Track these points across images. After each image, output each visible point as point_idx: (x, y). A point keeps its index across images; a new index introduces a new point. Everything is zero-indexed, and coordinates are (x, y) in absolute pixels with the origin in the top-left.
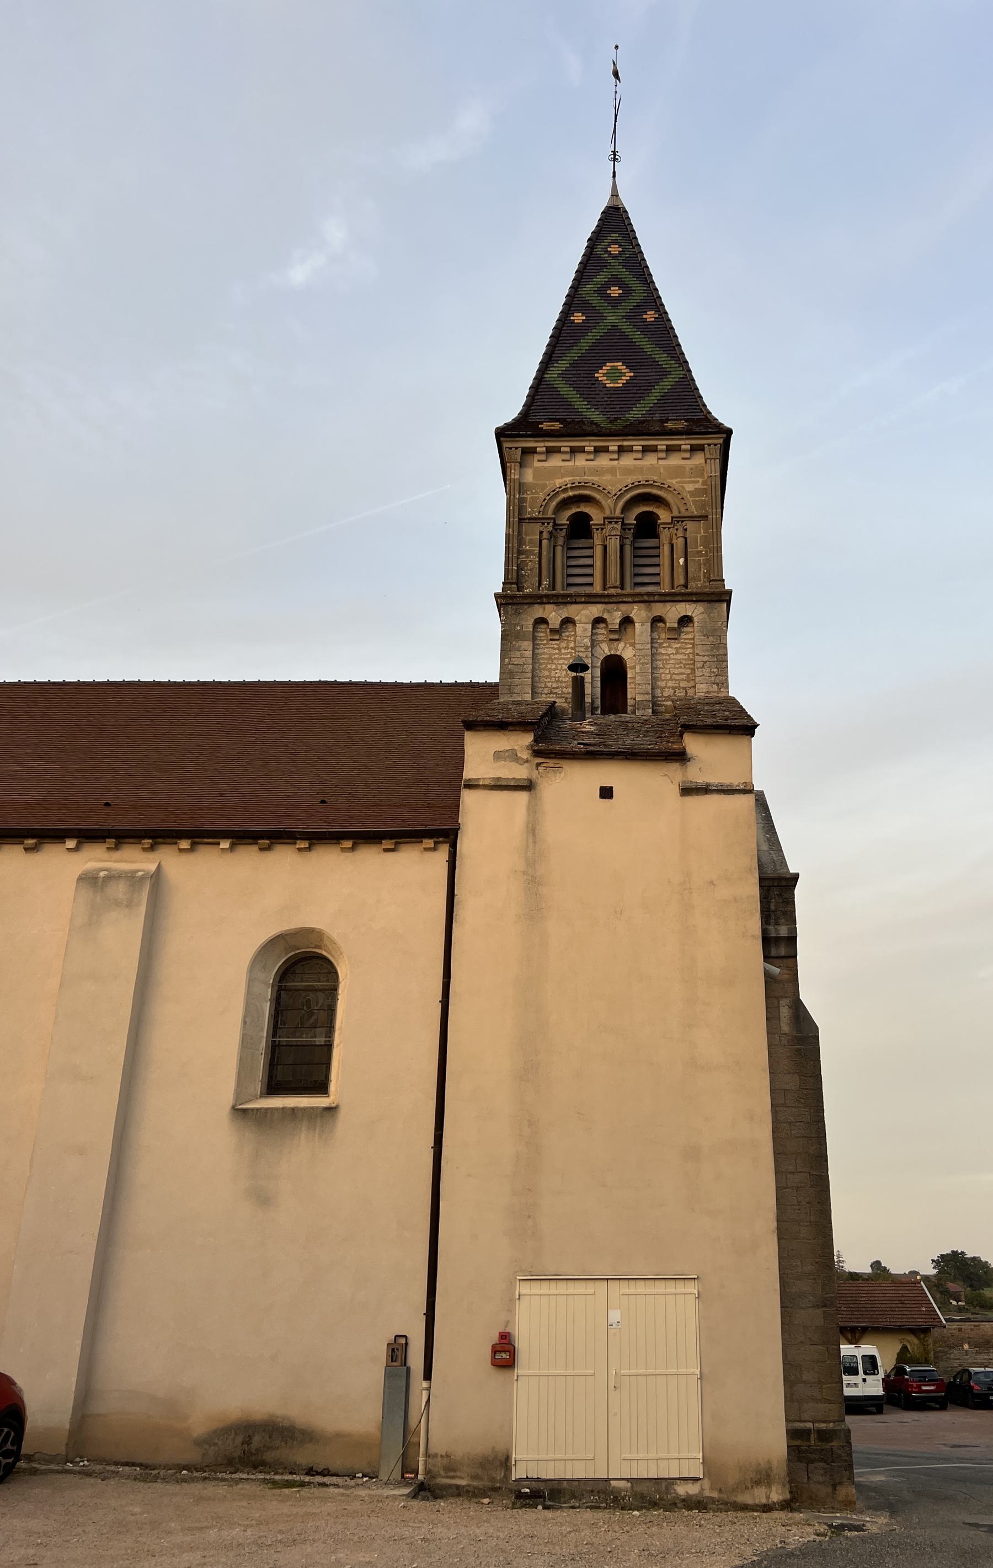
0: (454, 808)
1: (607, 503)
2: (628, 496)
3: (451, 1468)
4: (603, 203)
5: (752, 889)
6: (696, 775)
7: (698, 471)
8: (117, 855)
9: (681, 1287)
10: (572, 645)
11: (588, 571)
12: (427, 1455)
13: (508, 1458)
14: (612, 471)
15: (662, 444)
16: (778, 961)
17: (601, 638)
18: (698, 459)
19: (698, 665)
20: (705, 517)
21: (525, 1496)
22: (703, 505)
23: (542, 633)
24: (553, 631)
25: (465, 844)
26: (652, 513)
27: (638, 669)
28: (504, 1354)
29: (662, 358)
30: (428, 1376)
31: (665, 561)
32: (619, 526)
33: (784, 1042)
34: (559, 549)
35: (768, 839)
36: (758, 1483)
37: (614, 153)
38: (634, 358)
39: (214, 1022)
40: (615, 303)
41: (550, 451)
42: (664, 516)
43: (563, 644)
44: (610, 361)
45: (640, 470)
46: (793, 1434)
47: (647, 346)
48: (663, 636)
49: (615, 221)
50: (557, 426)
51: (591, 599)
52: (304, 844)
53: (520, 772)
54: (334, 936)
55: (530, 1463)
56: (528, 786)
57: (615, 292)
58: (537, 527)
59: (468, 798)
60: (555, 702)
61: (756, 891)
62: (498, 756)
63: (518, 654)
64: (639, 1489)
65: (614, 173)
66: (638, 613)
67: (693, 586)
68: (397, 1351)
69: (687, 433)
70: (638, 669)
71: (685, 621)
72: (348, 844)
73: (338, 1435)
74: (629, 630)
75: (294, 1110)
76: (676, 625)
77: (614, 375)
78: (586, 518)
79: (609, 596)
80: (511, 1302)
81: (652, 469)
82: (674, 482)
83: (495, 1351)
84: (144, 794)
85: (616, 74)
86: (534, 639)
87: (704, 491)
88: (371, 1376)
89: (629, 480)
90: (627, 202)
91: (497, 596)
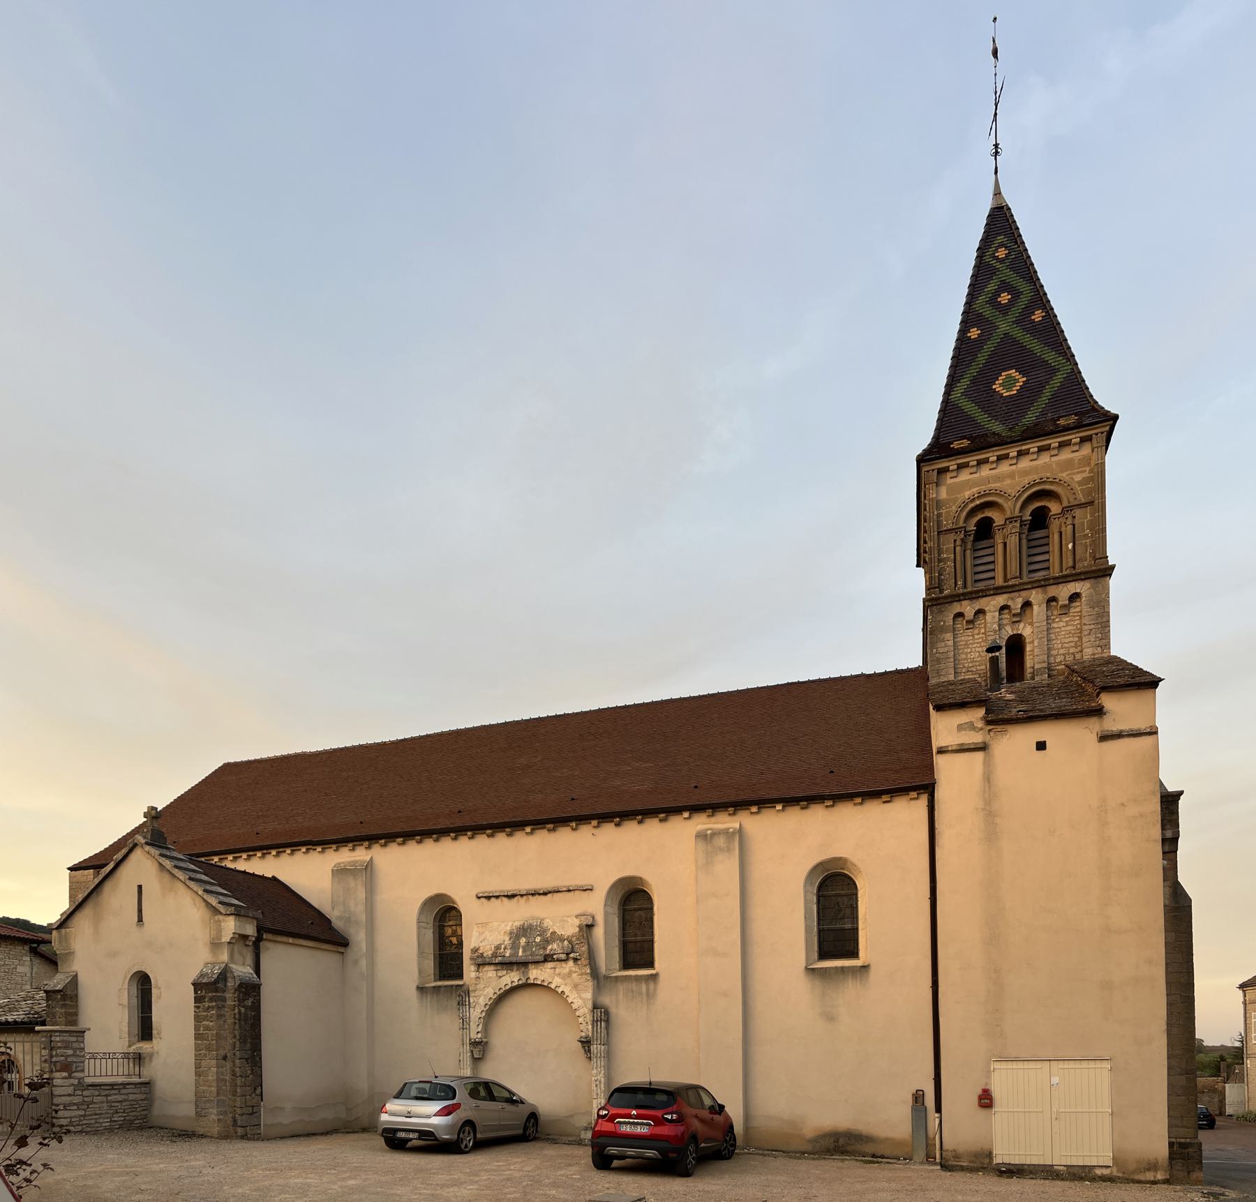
0: (930, 768)
1: (1007, 505)
2: (1025, 496)
3: (957, 1157)
5: (1157, 807)
6: (1110, 725)
8: (713, 819)
9: (1099, 1064)
11: (991, 567)
14: (1011, 475)
15: (1054, 442)
17: (1005, 622)
20: (1091, 503)
23: (961, 624)
24: (968, 622)
25: (940, 794)
26: (1045, 507)
27: (1036, 643)
28: (986, 1100)
29: (1051, 357)
30: (938, 1109)
32: (1018, 524)
34: (968, 552)
36: (1149, 1170)
37: (996, 146)
38: (1026, 362)
39: (788, 920)
40: (1004, 310)
41: (961, 467)
42: (1054, 508)
43: (976, 631)
45: (1036, 469)
46: (1171, 1145)
47: (1035, 346)
49: (1001, 223)
50: (966, 443)
51: (998, 591)
52: (830, 803)
53: (977, 738)
55: (1003, 1155)
56: (983, 748)
57: (1005, 298)
58: (952, 537)
59: (940, 761)
62: (960, 728)
64: (1075, 1171)
66: (1036, 597)
67: (1081, 567)
68: (918, 1097)
69: (1079, 426)
70: (1036, 643)
71: (1075, 597)
72: (859, 800)
73: (887, 1139)
74: (1028, 612)
75: (842, 968)
77: (1009, 383)
78: (989, 521)
80: (988, 1073)
81: (1047, 467)
83: (980, 1098)
86: (954, 630)
89: (1026, 481)
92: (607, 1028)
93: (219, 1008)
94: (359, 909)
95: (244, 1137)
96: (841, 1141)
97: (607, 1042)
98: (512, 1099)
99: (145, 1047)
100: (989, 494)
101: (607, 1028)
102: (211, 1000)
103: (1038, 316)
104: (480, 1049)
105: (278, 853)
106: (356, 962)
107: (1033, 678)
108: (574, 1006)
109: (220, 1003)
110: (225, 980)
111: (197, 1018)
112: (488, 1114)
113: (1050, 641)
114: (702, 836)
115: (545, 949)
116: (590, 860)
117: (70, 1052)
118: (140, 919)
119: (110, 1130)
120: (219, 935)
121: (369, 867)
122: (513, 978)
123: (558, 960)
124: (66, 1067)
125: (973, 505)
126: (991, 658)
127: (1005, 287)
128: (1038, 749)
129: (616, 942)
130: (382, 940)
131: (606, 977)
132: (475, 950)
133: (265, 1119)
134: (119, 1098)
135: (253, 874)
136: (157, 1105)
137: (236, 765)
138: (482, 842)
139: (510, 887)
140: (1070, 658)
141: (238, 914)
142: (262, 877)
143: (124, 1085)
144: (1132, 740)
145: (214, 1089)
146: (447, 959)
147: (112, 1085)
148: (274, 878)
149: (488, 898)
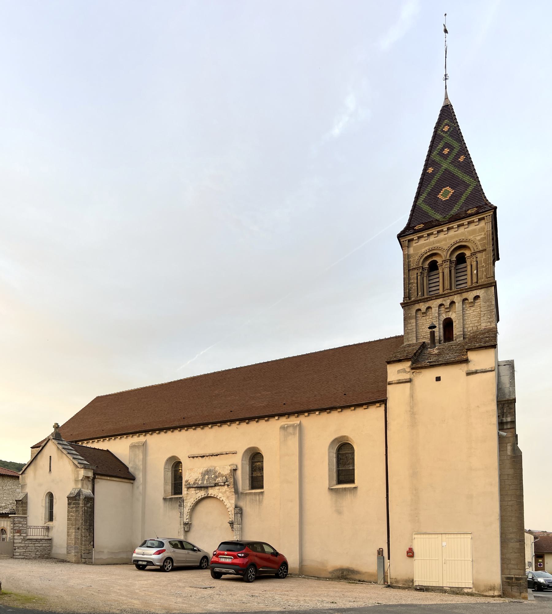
0: (385, 391)
1: (443, 254)
3: (397, 582)
5: (493, 407)
6: (472, 367)
7: (483, 229)
8: (289, 420)
9: (466, 536)
10: (431, 317)
11: (437, 284)
12: (390, 578)
13: (413, 580)
14: (445, 239)
15: (465, 222)
16: (507, 430)
17: (442, 312)
18: (482, 224)
19: (482, 315)
20: (485, 250)
21: (418, 589)
22: (484, 245)
24: (423, 313)
25: (390, 403)
27: (457, 322)
28: (411, 553)
29: (467, 179)
30: (389, 559)
31: (469, 272)
32: (448, 263)
33: (509, 458)
34: (425, 278)
35: (510, 382)
36: (491, 590)
40: (445, 157)
41: (419, 238)
42: (468, 253)
43: (428, 317)
44: (444, 187)
47: (459, 174)
48: (468, 306)
49: (447, 113)
51: (438, 297)
52: (340, 410)
53: (407, 376)
54: (352, 438)
55: (419, 581)
56: (410, 381)
58: (416, 271)
60: (424, 342)
61: (495, 407)
62: (399, 372)
63: (410, 325)
64: (452, 589)
65: (446, 86)
66: (457, 299)
67: (481, 282)
69: (477, 213)
70: (457, 322)
71: (477, 297)
72: (353, 408)
73: (366, 573)
76: (472, 301)
77: (446, 193)
78: (435, 262)
79: (445, 294)
80: (412, 540)
81: (463, 234)
82: (471, 237)
84: (294, 399)
85: (446, 31)
86: (416, 317)
87: (484, 238)
88: (374, 558)
89: (452, 242)
91: (401, 304)
92: (241, 517)
93: (76, 507)
94: (140, 464)
95: (85, 563)
96: (345, 573)
97: (241, 524)
98: (194, 549)
99: (50, 524)
101: (241, 517)
102: (74, 504)
103: (462, 159)
104: (188, 527)
105: (109, 439)
106: (138, 487)
107: (456, 340)
108: (227, 507)
109: (77, 505)
110: (80, 496)
111: (69, 512)
112: (180, 555)
113: (467, 319)
114: (283, 428)
115: (215, 480)
116: (230, 442)
117: (21, 525)
118: (50, 471)
119: (35, 558)
120: (78, 477)
121: (145, 444)
122: (202, 494)
123: (220, 486)
124: (19, 531)
125: (426, 255)
126: (431, 332)
127: (447, 145)
129: (247, 477)
130: (149, 477)
131: (242, 493)
132: (187, 481)
133: (95, 556)
134: (39, 545)
135: (98, 449)
136: (54, 548)
137: (102, 397)
138: (191, 432)
139: (202, 453)
140: (475, 329)
141: (85, 467)
142: (102, 450)
143: (41, 540)
144: (483, 374)
145: (73, 542)
146: (177, 484)
147: (36, 540)
148: (108, 451)
149: (193, 457)
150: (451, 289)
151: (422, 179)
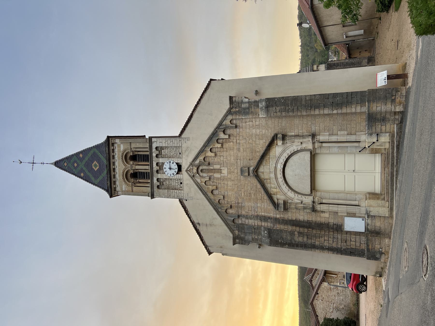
4: (306, 75)
14: (119, 169)
29: (92, 152)
34: (140, 181)
49: (58, 164)
77: (95, 166)
90: (54, 161)
91: (152, 198)
100: (123, 174)
128: (256, 91)
150: (148, 165)
151: (86, 180)
